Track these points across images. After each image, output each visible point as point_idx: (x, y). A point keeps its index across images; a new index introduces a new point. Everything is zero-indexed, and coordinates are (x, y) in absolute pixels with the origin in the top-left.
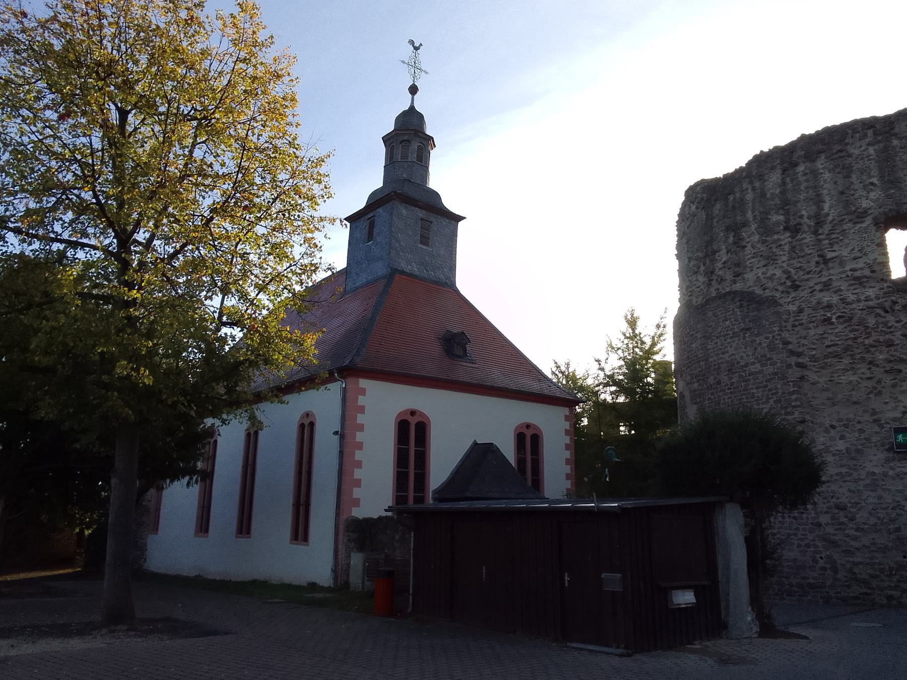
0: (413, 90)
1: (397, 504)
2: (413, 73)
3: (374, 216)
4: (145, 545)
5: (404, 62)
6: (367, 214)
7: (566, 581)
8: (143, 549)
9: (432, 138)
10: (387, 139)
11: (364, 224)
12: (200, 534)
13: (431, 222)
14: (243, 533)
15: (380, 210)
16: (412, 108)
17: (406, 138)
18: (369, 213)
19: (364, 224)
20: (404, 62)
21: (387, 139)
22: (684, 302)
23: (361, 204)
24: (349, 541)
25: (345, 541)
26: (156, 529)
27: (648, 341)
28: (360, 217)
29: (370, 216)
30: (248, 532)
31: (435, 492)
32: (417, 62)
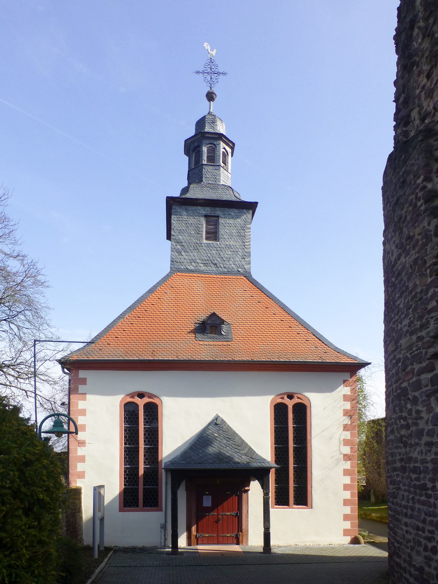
0: (210, 97)
13: (218, 217)
31: (165, 463)
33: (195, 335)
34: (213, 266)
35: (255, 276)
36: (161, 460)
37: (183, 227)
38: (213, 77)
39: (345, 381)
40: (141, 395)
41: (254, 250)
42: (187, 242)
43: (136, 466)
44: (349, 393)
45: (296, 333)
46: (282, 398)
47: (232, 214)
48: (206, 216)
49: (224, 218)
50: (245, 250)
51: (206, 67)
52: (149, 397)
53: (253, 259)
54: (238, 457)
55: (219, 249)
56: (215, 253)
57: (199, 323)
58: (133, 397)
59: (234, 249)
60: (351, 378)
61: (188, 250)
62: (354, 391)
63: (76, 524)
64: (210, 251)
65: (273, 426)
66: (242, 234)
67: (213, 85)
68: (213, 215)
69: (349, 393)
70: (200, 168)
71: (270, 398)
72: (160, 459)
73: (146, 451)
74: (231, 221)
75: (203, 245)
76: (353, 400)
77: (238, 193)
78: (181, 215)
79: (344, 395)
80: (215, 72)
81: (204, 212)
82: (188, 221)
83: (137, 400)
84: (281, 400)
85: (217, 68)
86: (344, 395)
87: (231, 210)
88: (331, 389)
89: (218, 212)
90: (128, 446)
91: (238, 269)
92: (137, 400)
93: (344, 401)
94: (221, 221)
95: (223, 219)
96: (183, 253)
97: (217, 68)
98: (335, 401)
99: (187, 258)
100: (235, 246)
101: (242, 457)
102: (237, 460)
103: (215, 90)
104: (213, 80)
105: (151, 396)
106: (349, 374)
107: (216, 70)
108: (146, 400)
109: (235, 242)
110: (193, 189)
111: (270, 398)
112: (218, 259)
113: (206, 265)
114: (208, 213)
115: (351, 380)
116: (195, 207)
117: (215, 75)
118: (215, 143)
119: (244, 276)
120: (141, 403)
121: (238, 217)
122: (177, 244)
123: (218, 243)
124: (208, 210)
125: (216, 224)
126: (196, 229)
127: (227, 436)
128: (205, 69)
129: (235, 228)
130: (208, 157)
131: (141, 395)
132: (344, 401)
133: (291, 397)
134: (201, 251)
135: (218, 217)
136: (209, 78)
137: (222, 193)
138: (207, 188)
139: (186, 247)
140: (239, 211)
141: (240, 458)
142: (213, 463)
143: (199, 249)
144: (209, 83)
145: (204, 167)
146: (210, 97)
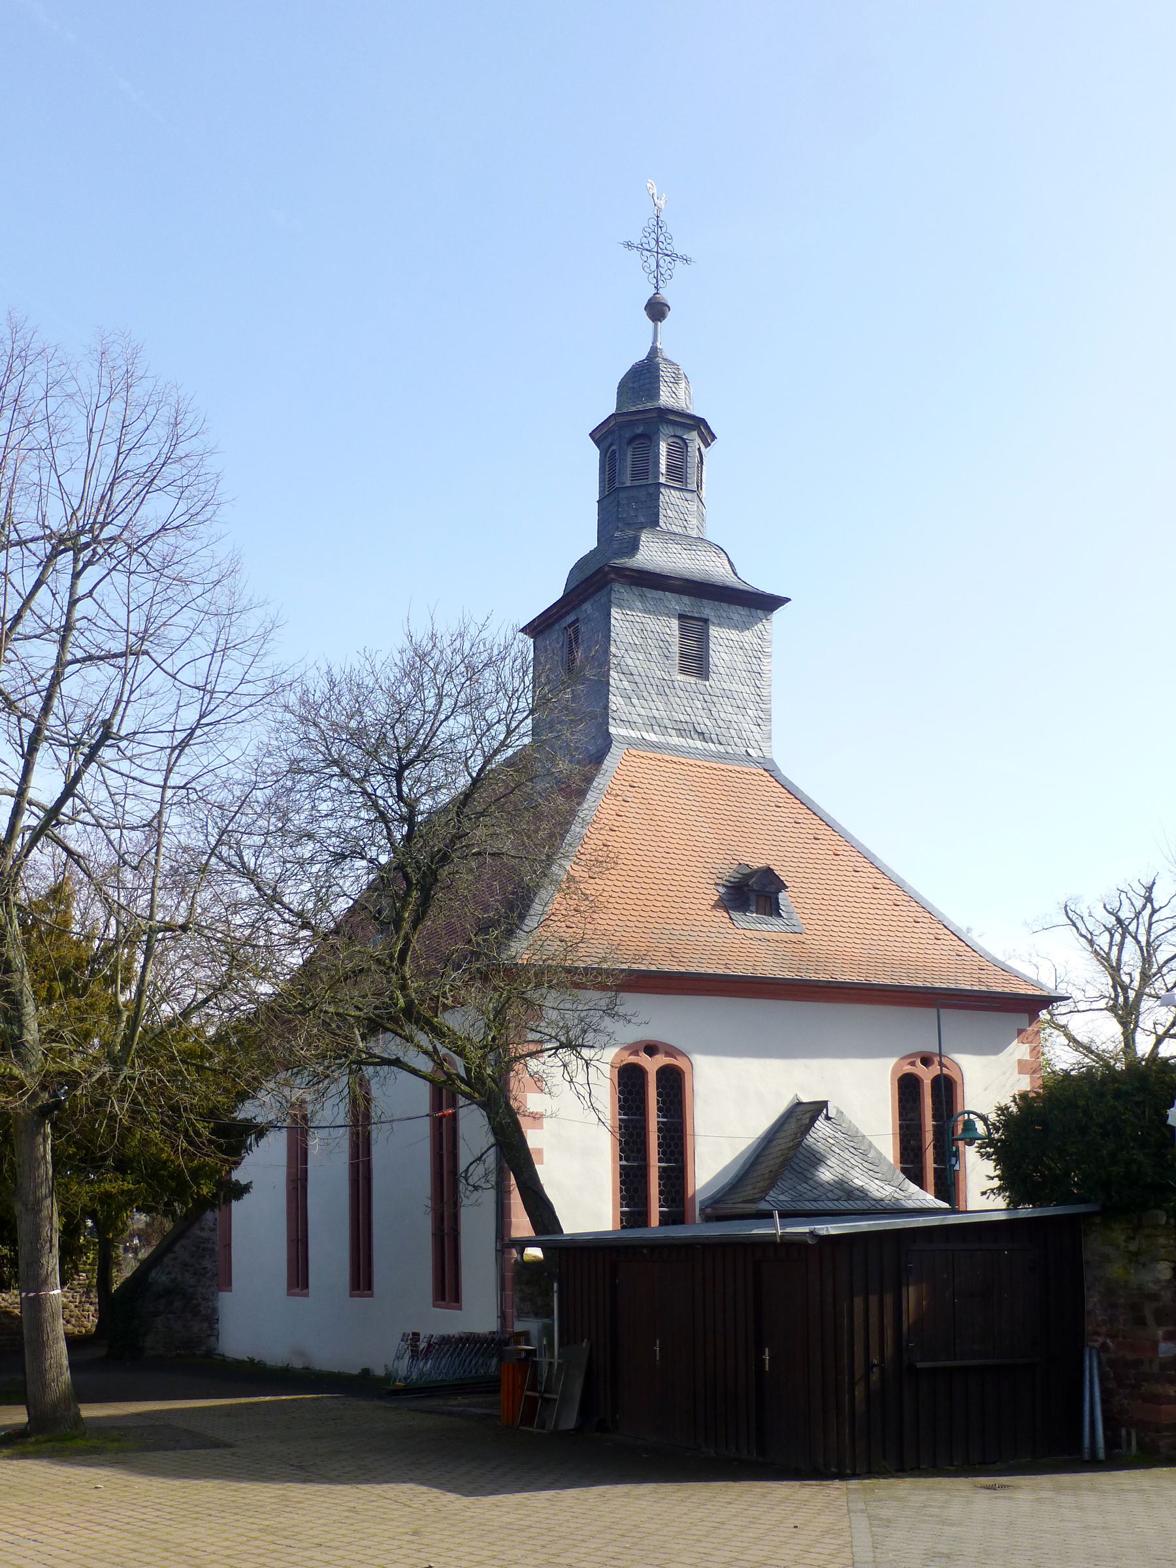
0: (656, 310)
1: (623, 1227)
2: (654, 267)
3: (577, 620)
4: (214, 1310)
5: (629, 245)
6: (562, 617)
7: (767, 1353)
8: (211, 1319)
9: (703, 421)
10: (600, 436)
11: (556, 638)
12: (297, 1290)
13: (706, 621)
14: (447, 1299)
15: (587, 607)
16: (654, 352)
17: (640, 430)
18: (568, 613)
19: (556, 638)
20: (629, 245)
21: (600, 436)
22: (760, 613)
23: (554, 592)
24: (522, 1300)
25: (516, 1300)
26: (227, 1284)
27: (244, 602)
28: (553, 624)
29: (570, 619)
30: (369, 1286)
31: (701, 1202)
32: (661, 238)
33: (728, 913)
34: (695, 736)
35: (788, 771)
36: (694, 1196)
37: (634, 637)
38: (661, 262)
39: (1020, 1032)
40: (651, 1049)
41: (777, 709)
42: (643, 674)
43: (643, 1209)
44: (1027, 1057)
45: (607, 828)
46: (913, 1064)
47: (736, 617)
48: (682, 617)
49: (720, 625)
50: (761, 705)
51: (647, 235)
52: (668, 1054)
53: (777, 726)
54: (876, 1187)
55: (707, 698)
56: (700, 707)
57: (724, 886)
58: (636, 1053)
59: (739, 701)
60: (1030, 1025)
61: (645, 694)
62: (1035, 1052)
63: (487, 1339)
64: (690, 701)
65: (898, 1122)
66: (753, 666)
67: (660, 283)
68: (696, 615)
69: (1027, 1057)
70: (651, 490)
71: (892, 1062)
72: (690, 1193)
73: (664, 1174)
74: (734, 634)
75: (676, 684)
76: (1034, 1072)
77: (729, 560)
78: (630, 609)
79: (1020, 1061)
80: (665, 252)
81: (677, 607)
82: (645, 625)
83: (644, 1060)
84: (909, 1067)
85: (669, 241)
86: (1020, 1061)
87: (733, 607)
88: (996, 1048)
89: (707, 609)
90: (624, 1163)
91: (749, 750)
92: (644, 1060)
93: (1020, 1073)
94: (714, 631)
95: (718, 629)
96: (635, 701)
97: (669, 241)
98: (1004, 1074)
99: (642, 712)
100: (740, 694)
101: (885, 1187)
102: (878, 1195)
103: (666, 295)
104: (663, 271)
105: (671, 1051)
106: (1025, 1017)
107: (668, 246)
108: (661, 1060)
109: (740, 685)
110: (647, 544)
111: (892, 1062)
112: (707, 721)
113: (683, 732)
114: (687, 610)
115: (1030, 1029)
116: (660, 593)
117: (666, 258)
118: (685, 437)
119: (765, 770)
120: (652, 1065)
121: (744, 626)
122: (622, 676)
123: (707, 683)
124: (685, 604)
125: (703, 640)
126: (661, 644)
127: (852, 1144)
128: (645, 240)
129: (740, 652)
130: (669, 467)
131: (651, 1049)
132: (1020, 1073)
133: (926, 1061)
134: (672, 699)
135: (706, 621)
136: (652, 262)
137: (707, 563)
138: (676, 546)
139: (642, 687)
140: (748, 613)
141: (881, 1190)
142: (837, 1200)
143: (669, 693)
144: (652, 275)
145: (662, 490)
146: (656, 310)
